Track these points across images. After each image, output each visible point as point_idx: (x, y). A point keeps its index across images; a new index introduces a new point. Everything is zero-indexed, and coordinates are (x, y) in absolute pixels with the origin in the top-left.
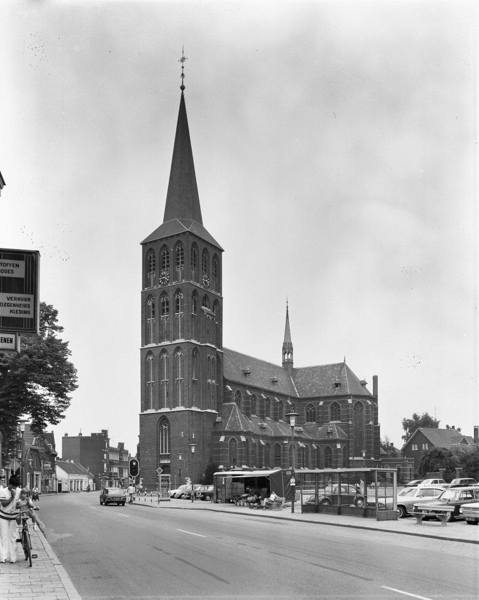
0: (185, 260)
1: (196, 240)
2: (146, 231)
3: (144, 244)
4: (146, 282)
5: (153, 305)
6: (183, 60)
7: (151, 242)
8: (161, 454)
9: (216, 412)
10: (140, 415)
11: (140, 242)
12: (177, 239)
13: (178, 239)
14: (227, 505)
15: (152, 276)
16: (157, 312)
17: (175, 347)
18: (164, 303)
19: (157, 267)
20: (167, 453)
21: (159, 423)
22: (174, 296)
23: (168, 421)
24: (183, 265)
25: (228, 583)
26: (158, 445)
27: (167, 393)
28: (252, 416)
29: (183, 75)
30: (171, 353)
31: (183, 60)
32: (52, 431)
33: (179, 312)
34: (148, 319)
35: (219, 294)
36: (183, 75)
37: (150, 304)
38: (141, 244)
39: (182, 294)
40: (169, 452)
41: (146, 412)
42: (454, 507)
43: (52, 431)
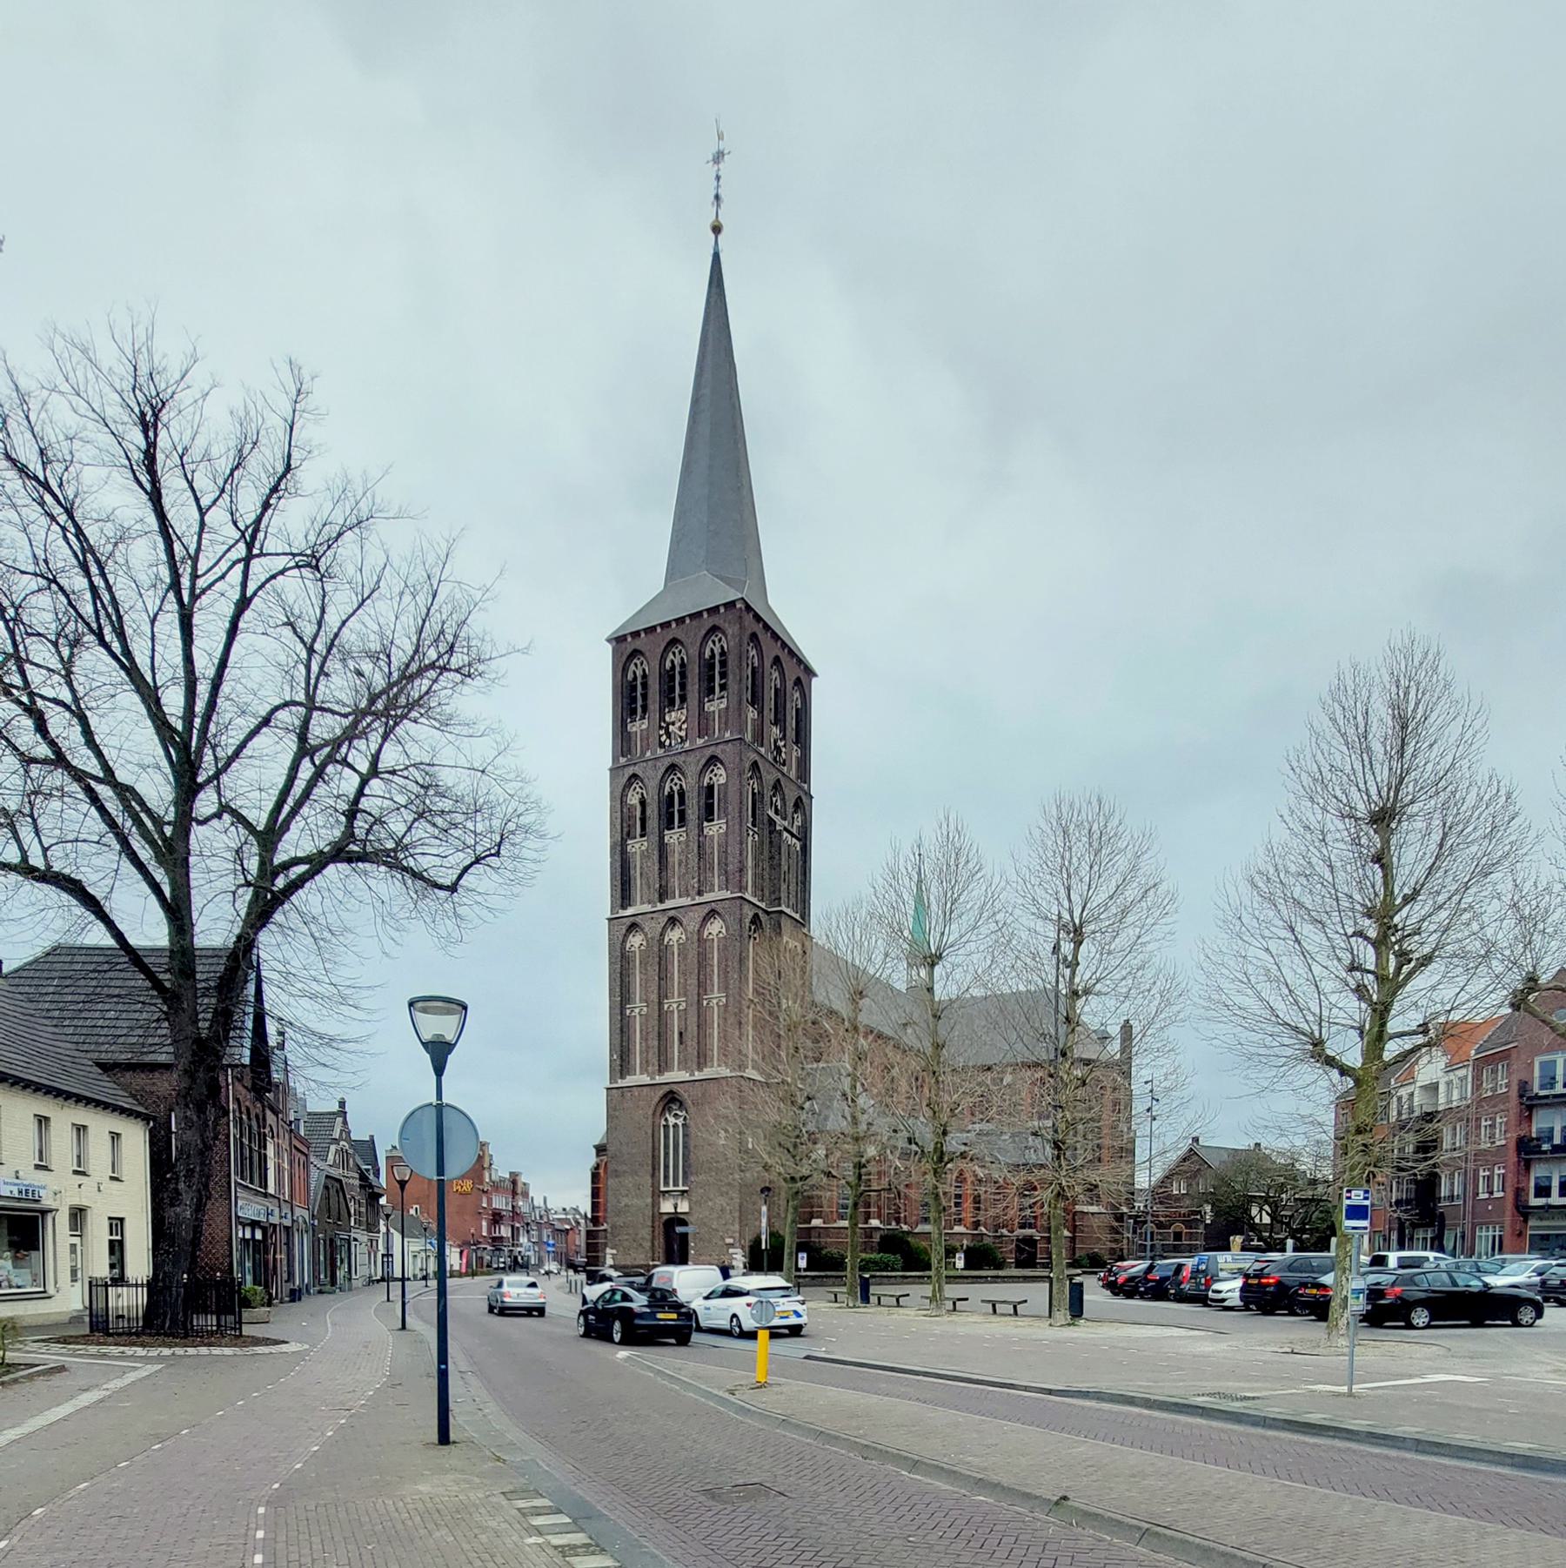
0: (733, 685)
1: (758, 628)
2: (619, 613)
3: (618, 640)
4: (623, 741)
5: (643, 803)
6: (719, 157)
7: (636, 634)
8: (662, 1189)
9: (161, 1366)
10: (608, 1089)
11: (606, 637)
12: (708, 622)
13: (711, 620)
14: (1295, 1322)
15: (638, 727)
16: (653, 824)
17: (707, 909)
18: (671, 796)
19: (654, 706)
20: (681, 1188)
21: (662, 1104)
22: (702, 773)
23: (681, 1105)
24: (724, 693)
25: (287, 1342)
26: (655, 1168)
27: (681, 1034)
28: (1397, 919)
29: (717, 197)
30: (693, 926)
31: (719, 157)
32: (372, 1137)
33: (713, 820)
34: (629, 842)
35: (806, 786)
36: (717, 197)
37: (633, 799)
38: (609, 640)
39: (722, 771)
40: (683, 1185)
41: (621, 1083)
42: (247, 1330)
43: (372, 1137)
